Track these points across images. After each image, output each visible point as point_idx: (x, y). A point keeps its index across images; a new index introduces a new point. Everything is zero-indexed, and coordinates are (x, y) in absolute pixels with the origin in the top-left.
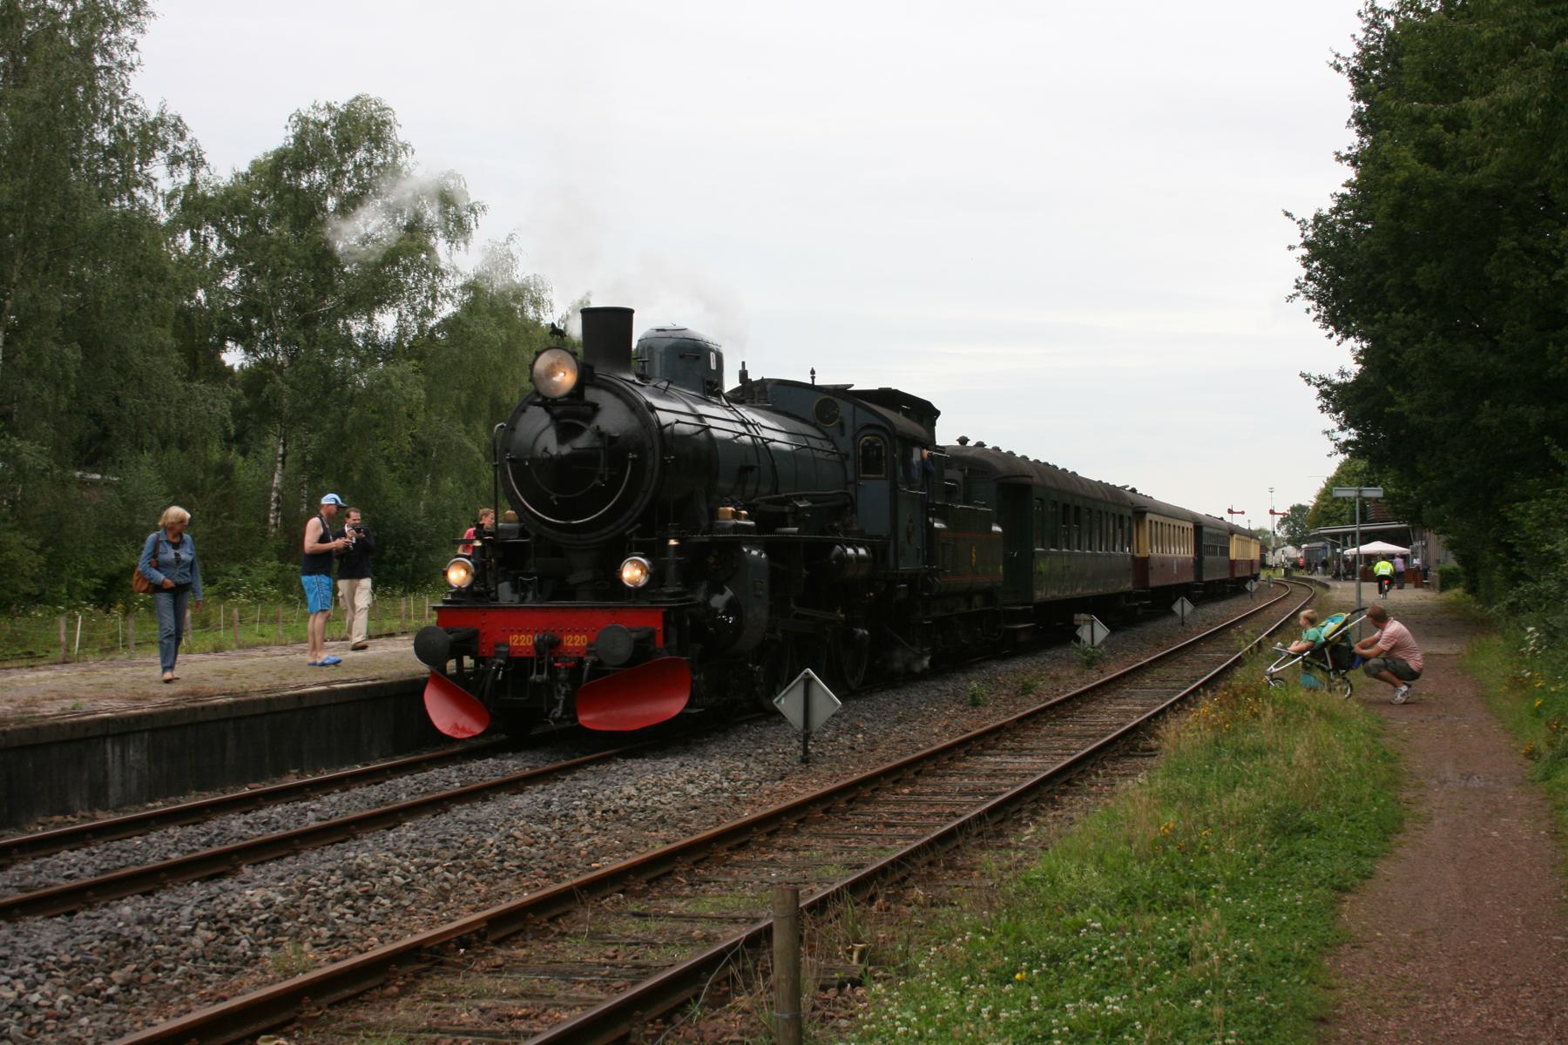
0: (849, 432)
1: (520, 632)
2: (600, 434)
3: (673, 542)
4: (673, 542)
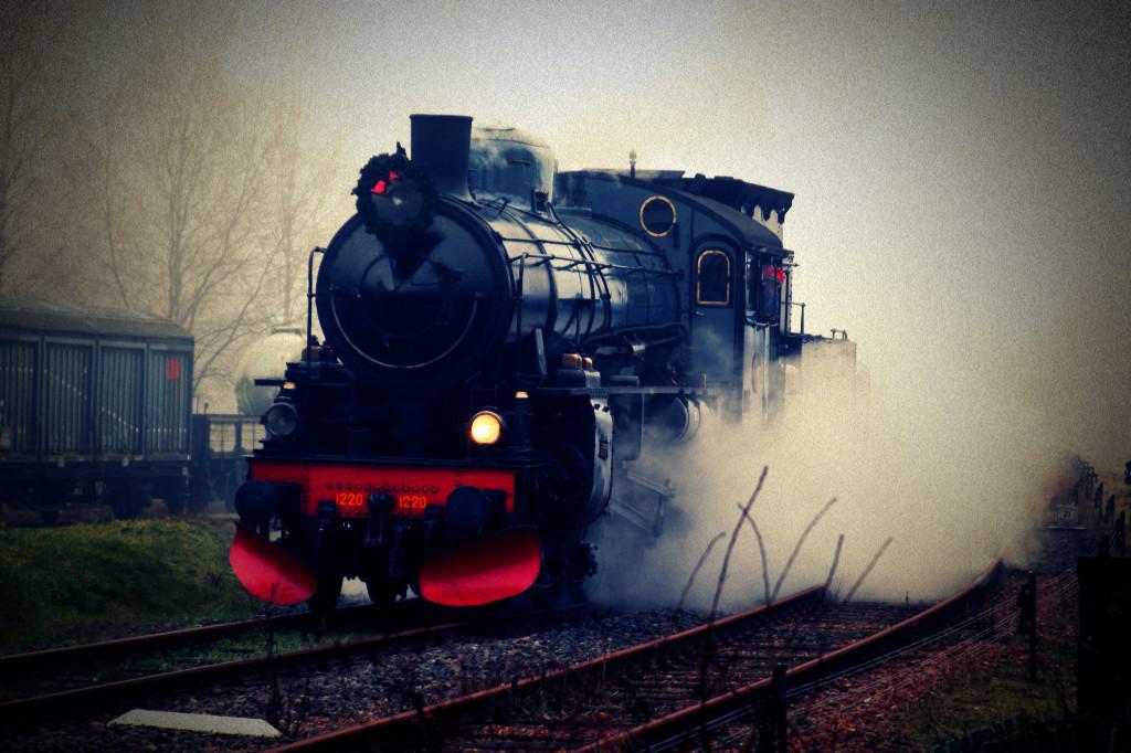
0: (685, 243)
1: (349, 490)
2: (441, 270)
3: (522, 395)
4: (522, 395)
